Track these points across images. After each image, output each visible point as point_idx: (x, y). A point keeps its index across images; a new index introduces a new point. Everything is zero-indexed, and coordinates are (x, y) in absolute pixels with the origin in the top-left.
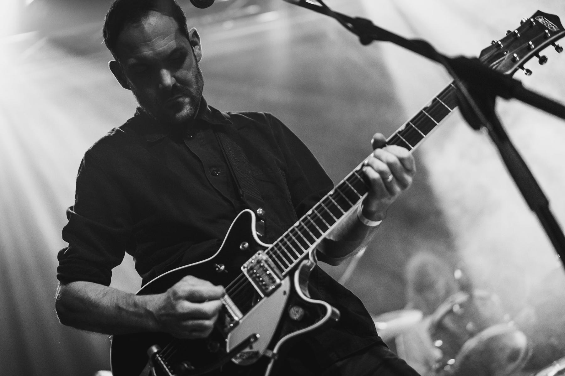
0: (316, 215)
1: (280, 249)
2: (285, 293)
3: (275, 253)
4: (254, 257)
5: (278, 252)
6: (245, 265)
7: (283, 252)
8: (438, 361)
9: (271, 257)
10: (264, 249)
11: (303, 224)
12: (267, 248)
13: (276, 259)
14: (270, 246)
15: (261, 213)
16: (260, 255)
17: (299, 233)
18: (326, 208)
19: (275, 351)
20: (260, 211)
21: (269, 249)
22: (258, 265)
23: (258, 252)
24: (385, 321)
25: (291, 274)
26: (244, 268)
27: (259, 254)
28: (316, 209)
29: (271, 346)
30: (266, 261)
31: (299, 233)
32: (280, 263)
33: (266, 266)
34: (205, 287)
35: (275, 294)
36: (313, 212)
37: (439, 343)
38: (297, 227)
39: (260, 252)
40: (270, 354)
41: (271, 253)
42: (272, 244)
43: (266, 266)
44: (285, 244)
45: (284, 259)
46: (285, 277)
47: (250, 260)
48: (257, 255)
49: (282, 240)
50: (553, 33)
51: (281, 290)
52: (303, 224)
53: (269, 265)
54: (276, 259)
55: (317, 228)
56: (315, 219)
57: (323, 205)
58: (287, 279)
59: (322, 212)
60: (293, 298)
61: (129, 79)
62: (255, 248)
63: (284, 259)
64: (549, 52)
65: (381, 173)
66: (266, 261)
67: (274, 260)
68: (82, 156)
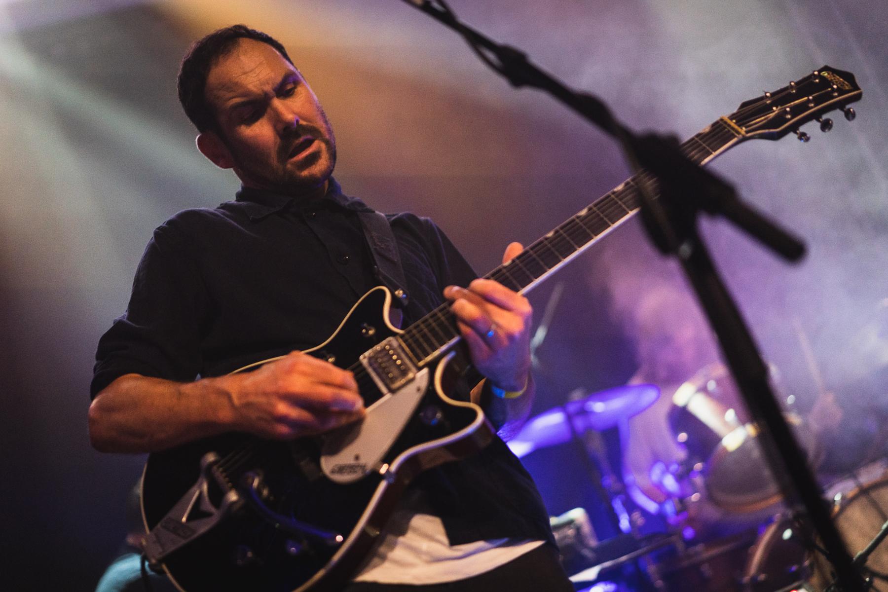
2: (419, 390)
6: (367, 354)
8: (681, 464)
10: (394, 334)
15: (401, 292)
19: (394, 467)
24: (602, 400)
25: (432, 366)
26: (365, 357)
29: (388, 458)
35: (404, 391)
37: (683, 437)
40: (383, 469)
50: (841, 91)
51: (412, 388)
58: (425, 371)
60: (429, 397)
61: (297, 142)
62: (384, 333)
64: (812, 128)
65: (218, 468)
68: (148, 237)
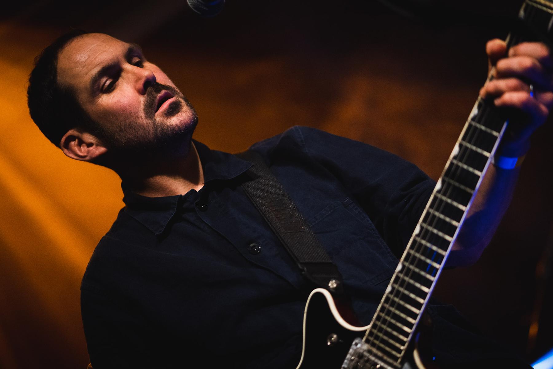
0: (427, 231)
1: (381, 330)
3: (377, 337)
4: (351, 351)
5: (388, 318)
7: (387, 333)
9: (373, 345)
10: (361, 334)
11: (396, 286)
12: (365, 331)
13: (382, 345)
14: (368, 327)
15: (335, 285)
16: (359, 346)
17: (407, 279)
18: (418, 255)
20: (333, 284)
21: (367, 333)
22: (362, 361)
23: (354, 343)
27: (356, 344)
28: (424, 221)
30: (369, 352)
31: (407, 279)
32: (388, 349)
33: (373, 358)
34: (175, 121)
36: (422, 228)
38: (401, 272)
39: (356, 341)
41: (371, 339)
42: (369, 324)
43: (373, 358)
44: (389, 313)
45: (391, 341)
46: (402, 363)
47: (348, 356)
48: (353, 347)
49: (378, 318)
52: (396, 286)
53: (376, 356)
54: (382, 345)
55: (429, 261)
56: (428, 237)
57: (412, 252)
59: (428, 237)
62: (349, 337)
63: (391, 341)
66: (369, 352)
67: (379, 349)
